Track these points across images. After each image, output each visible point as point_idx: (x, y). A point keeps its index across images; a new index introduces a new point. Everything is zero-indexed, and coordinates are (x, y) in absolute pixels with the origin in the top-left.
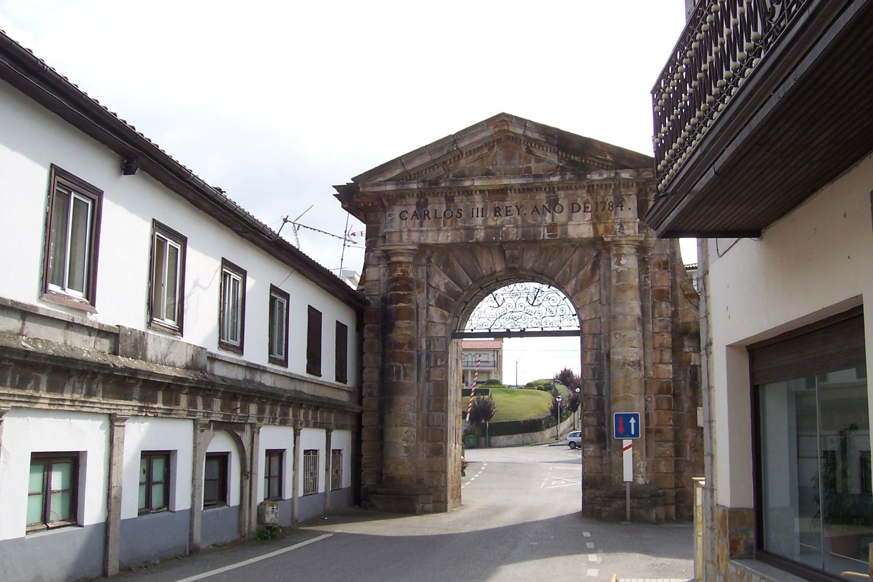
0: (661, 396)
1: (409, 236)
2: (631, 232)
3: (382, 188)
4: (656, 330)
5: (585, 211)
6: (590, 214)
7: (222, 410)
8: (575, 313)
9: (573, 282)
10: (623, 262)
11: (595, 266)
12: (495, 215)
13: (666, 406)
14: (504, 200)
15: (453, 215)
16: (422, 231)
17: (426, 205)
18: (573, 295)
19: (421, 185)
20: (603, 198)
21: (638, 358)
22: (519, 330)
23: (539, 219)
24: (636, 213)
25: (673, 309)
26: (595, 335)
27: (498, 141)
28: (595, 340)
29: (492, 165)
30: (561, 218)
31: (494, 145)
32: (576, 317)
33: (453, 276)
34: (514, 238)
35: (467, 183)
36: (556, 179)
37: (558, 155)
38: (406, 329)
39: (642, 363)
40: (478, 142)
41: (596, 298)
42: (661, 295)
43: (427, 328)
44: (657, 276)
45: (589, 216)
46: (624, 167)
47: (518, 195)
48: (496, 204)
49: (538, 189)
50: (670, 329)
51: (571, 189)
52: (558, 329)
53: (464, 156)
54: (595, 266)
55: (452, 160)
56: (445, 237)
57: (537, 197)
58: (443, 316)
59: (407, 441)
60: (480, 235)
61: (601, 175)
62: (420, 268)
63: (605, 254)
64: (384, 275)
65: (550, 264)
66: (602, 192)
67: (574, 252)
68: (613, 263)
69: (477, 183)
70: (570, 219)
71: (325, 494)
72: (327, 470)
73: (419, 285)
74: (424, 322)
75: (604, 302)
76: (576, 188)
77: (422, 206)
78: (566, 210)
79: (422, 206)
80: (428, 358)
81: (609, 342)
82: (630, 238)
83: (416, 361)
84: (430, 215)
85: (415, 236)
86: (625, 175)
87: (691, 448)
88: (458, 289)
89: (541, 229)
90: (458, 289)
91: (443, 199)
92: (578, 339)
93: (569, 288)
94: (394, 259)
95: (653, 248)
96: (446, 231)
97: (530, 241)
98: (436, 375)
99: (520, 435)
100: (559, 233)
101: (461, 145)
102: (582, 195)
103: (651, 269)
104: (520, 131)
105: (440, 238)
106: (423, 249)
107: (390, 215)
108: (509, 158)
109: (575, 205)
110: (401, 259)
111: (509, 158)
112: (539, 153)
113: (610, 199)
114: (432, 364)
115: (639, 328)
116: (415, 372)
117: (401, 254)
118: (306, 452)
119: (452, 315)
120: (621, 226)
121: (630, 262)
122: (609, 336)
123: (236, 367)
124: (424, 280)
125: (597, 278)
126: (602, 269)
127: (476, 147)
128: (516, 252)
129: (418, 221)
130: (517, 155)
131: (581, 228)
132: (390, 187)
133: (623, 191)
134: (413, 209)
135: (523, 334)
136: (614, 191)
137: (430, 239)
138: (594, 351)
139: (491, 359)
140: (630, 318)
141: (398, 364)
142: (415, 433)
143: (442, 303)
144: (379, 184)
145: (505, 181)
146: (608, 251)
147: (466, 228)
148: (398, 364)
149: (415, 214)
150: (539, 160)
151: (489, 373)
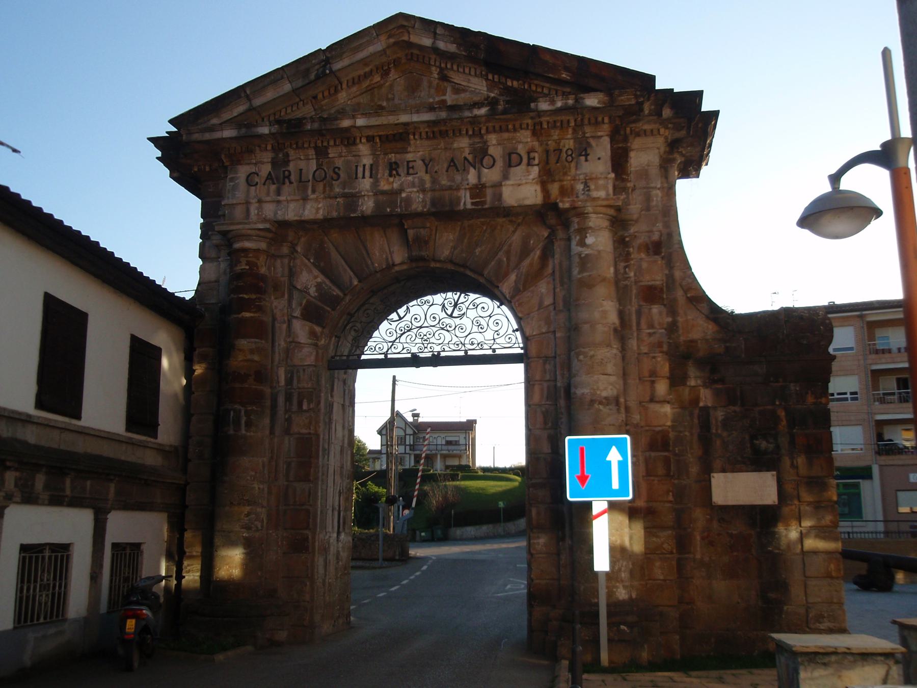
0: (653, 454)
1: (260, 209)
2: (602, 194)
3: (217, 135)
4: (645, 349)
6: (536, 169)
8: (516, 327)
9: (513, 277)
10: (590, 240)
11: (547, 254)
12: (391, 175)
13: (661, 471)
14: (405, 151)
15: (327, 177)
16: (279, 202)
17: (286, 162)
18: (513, 297)
19: (275, 128)
20: (558, 142)
21: (615, 392)
22: (429, 355)
23: (458, 178)
24: (609, 164)
25: (670, 319)
26: (546, 359)
27: (396, 63)
28: (548, 367)
29: (388, 100)
30: (491, 175)
31: (389, 69)
32: (518, 334)
33: (327, 271)
34: (420, 209)
35: (346, 123)
36: (483, 111)
37: (487, 79)
38: (252, 352)
39: (622, 400)
40: (364, 62)
41: (548, 301)
42: (651, 295)
43: (287, 351)
44: (645, 265)
45: (535, 171)
46: (589, 90)
47: (426, 143)
48: (393, 157)
49: (457, 133)
50: (665, 348)
51: (507, 130)
52: (490, 352)
53: (344, 86)
54: (547, 254)
55: (326, 93)
56: (314, 209)
57: (455, 145)
58: (313, 334)
59: (248, 528)
60: (367, 206)
61: (553, 102)
62: (279, 261)
63: (561, 234)
64: (225, 273)
65: (478, 251)
66: (556, 134)
67: (514, 232)
68: (574, 243)
69: (360, 122)
70: (506, 177)
72: (95, 577)
73: (276, 287)
74: (283, 343)
75: (561, 306)
76: (515, 130)
77: (280, 163)
78: (500, 164)
79: (280, 163)
80: (288, 398)
81: (569, 369)
82: (600, 203)
83: (268, 403)
84: (293, 178)
85: (269, 210)
86: (592, 101)
87: (703, 538)
88: (336, 292)
89: (462, 193)
90: (336, 292)
91: (312, 152)
92: (520, 368)
93: (506, 287)
94: (237, 246)
95: (637, 221)
96: (316, 200)
97: (444, 213)
98: (300, 425)
99: (491, 526)
100: (489, 199)
101: (337, 66)
102: (524, 140)
103: (637, 256)
104: (427, 42)
105: (306, 212)
106: (281, 230)
107: (232, 180)
108: (413, 88)
109: (514, 156)
110: (247, 244)
111: (413, 88)
112: (458, 79)
113: (569, 143)
114: (295, 407)
115: (616, 345)
116: (267, 421)
117: (247, 237)
118: (115, 546)
119: (326, 331)
120: (586, 184)
121: (599, 240)
122: (569, 359)
124: (285, 279)
125: (549, 269)
126: (557, 256)
127: (361, 72)
128: (423, 232)
129: (273, 188)
130: (425, 83)
131: (523, 190)
132: (228, 133)
133: (589, 131)
134: (266, 169)
135: (437, 360)
136: (575, 131)
137: (291, 213)
138: (545, 385)
140: (600, 328)
141: (237, 406)
142: (264, 516)
143: (312, 314)
144: (212, 129)
145: (404, 118)
146: (566, 225)
147: (345, 196)
148: (237, 406)
149: (269, 177)
150: (458, 90)
151: (460, 457)
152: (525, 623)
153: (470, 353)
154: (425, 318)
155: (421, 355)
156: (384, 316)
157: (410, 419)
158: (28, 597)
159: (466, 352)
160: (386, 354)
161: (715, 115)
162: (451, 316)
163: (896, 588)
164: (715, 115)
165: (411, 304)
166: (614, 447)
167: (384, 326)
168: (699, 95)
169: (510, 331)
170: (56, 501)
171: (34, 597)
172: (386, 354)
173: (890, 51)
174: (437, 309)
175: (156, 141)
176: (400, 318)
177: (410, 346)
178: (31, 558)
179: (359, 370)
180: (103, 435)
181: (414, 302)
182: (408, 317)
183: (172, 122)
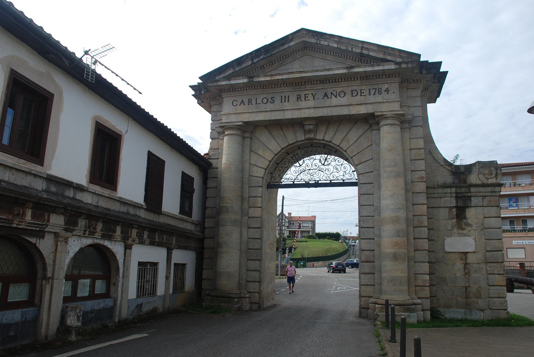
3: (220, 83)
5: (361, 95)
7: (65, 224)
8: (354, 169)
22: (314, 182)
32: (355, 173)
71: (164, 297)
72: (167, 278)
118: (175, 264)
123: (14, 172)
135: (317, 185)
139: (310, 225)
152: (358, 305)
154: (311, 166)
155: (310, 182)
156: (292, 164)
157: (287, 215)
158: (141, 286)
160: (294, 182)
161: (446, 73)
162: (324, 165)
164: (446, 73)
165: (305, 159)
167: (293, 169)
168: (439, 64)
169: (351, 172)
170: (152, 243)
171: (144, 285)
173: (207, 78)
174: (317, 162)
175: (192, 87)
176: (300, 166)
177: (305, 177)
178: (142, 269)
179: (279, 189)
180: (170, 215)
181: (307, 158)
182: (304, 165)
183: (200, 78)
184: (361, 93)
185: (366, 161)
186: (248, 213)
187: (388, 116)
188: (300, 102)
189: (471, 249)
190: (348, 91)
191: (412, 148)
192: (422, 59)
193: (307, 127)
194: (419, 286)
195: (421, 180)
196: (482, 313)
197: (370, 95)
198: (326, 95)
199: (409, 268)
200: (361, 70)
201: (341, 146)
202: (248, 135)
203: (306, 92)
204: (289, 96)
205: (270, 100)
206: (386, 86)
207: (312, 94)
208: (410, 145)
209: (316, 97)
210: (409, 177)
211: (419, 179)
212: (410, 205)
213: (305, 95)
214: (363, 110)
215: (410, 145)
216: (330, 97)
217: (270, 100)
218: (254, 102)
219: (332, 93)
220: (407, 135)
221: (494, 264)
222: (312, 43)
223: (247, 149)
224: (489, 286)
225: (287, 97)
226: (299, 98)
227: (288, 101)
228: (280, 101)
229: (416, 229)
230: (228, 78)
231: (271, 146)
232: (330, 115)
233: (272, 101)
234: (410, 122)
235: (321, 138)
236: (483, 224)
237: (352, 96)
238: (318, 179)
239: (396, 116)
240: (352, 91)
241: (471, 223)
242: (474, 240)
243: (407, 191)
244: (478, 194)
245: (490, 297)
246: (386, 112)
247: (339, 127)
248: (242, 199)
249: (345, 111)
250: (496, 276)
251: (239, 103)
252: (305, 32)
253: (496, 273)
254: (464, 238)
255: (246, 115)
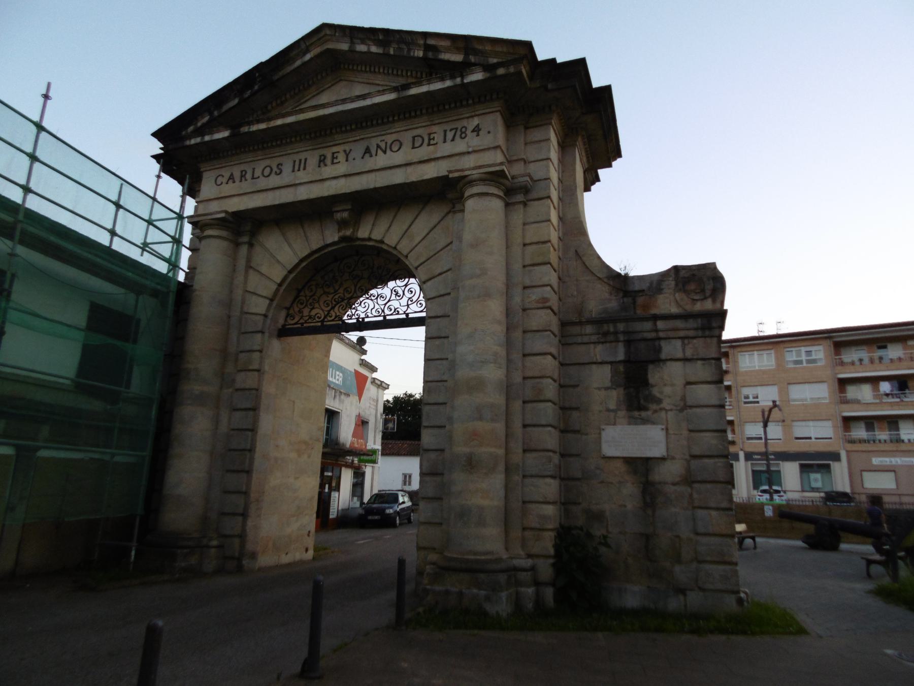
5: (429, 145)
153: (388, 318)
159: (385, 317)
163: (805, 475)
166: (726, 335)
168: (581, 64)
172: (322, 321)
184: (430, 139)
185: (440, 274)
186: (234, 381)
187: (474, 177)
188: (324, 169)
189: (658, 451)
190: (407, 137)
191: (528, 241)
192: (541, 56)
193: (338, 216)
194: (532, 529)
195: (541, 305)
196: (681, 597)
197: (445, 141)
198: (367, 151)
199: (508, 488)
200: (424, 89)
201: (398, 247)
202: (245, 239)
203: (335, 149)
204: (306, 160)
205: (275, 169)
206: (476, 121)
207: (345, 151)
208: (524, 236)
209: (350, 158)
210: (517, 299)
211: (538, 302)
212: (516, 356)
213: (333, 153)
214: (430, 172)
215: (524, 236)
216: (374, 152)
217: (275, 169)
218: (249, 176)
219: (378, 146)
220: (518, 216)
221: (709, 486)
222: (341, 51)
223: (242, 263)
224: (697, 534)
225: (303, 162)
226: (322, 161)
227: (304, 169)
228: (291, 169)
229: (529, 405)
230: (200, 132)
231: (282, 253)
232: (372, 186)
233: (278, 171)
234: (526, 190)
235: (366, 235)
236: (683, 398)
237: (413, 148)
238: (363, 315)
239: (483, 176)
240: (414, 138)
241: (658, 395)
242: (664, 432)
243: (510, 328)
244: (671, 334)
245: (700, 562)
246: (469, 169)
247: (399, 210)
248: (224, 354)
249: (398, 177)
250: (714, 513)
251: (225, 180)
252: (328, 32)
253: (713, 505)
254: (642, 428)
255: (236, 200)
